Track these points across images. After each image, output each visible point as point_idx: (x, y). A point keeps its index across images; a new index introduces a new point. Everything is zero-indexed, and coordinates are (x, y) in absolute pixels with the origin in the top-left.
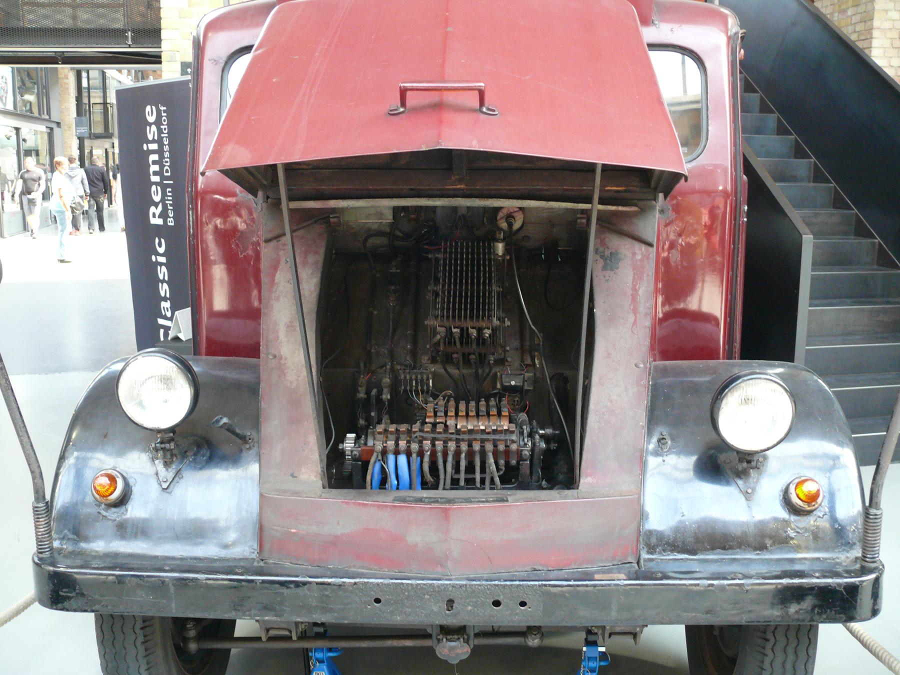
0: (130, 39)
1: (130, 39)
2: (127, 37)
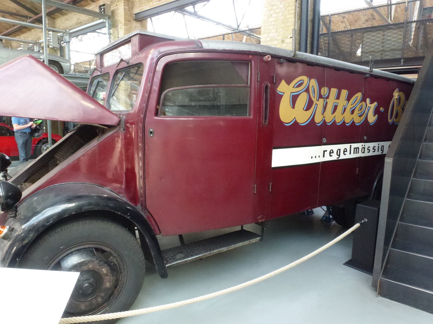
0: (402, 63)
1: (402, 63)
2: (401, 62)
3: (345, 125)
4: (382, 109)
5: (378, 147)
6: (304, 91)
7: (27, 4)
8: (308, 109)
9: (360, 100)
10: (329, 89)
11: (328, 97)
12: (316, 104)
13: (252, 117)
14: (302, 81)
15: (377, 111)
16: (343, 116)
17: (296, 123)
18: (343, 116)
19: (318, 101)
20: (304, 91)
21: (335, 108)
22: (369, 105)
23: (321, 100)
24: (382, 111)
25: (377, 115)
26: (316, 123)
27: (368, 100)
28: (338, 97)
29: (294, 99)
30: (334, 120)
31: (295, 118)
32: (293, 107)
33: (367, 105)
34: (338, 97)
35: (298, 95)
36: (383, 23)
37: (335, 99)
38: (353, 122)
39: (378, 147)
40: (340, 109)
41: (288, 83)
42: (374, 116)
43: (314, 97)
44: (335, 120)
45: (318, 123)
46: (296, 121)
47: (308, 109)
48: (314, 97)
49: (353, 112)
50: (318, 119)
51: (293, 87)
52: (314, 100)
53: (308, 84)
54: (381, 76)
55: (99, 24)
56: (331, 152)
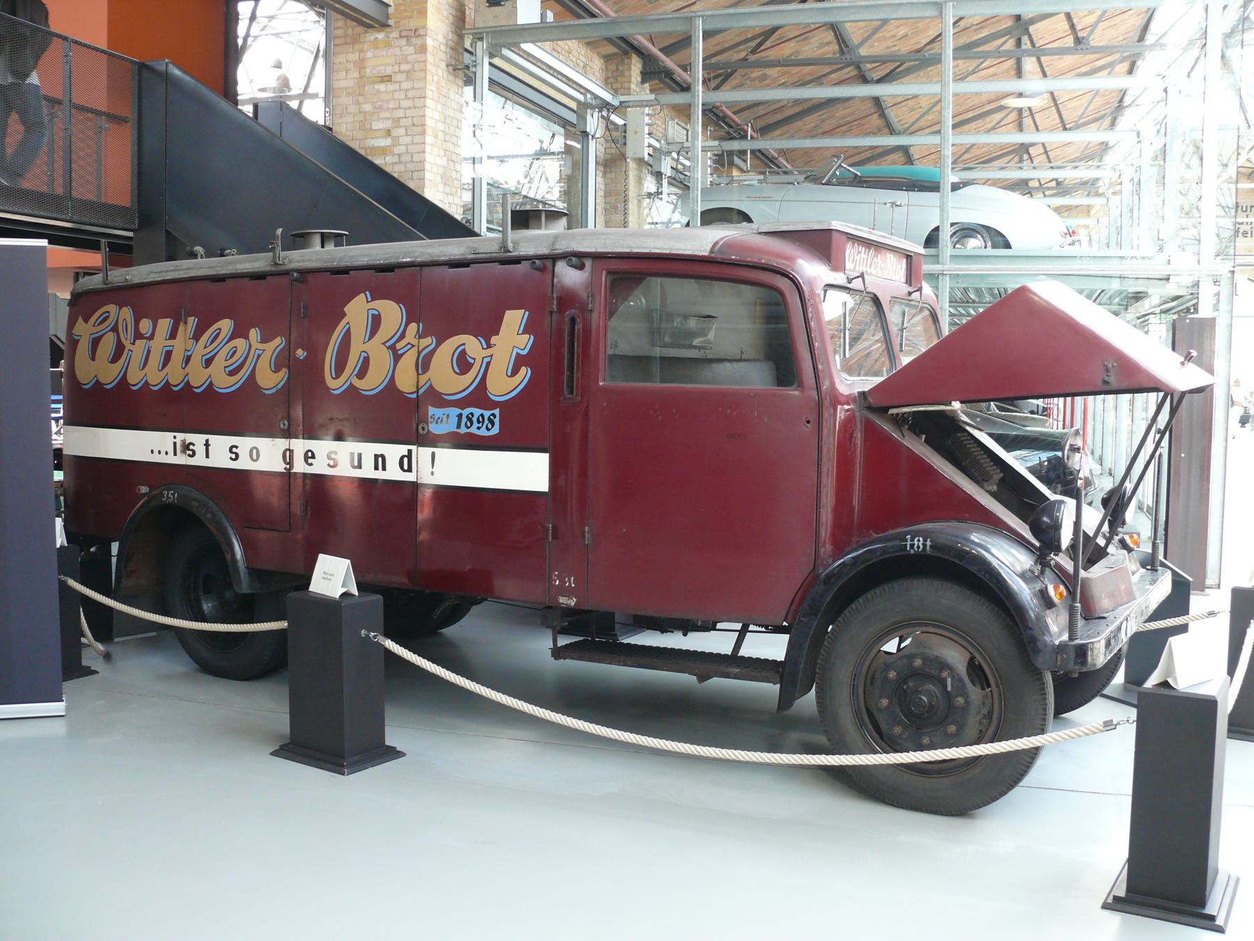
3: (193, 391)
4: (301, 353)
5: (175, 443)
6: (110, 331)
7: (307, 263)
8: (115, 359)
9: (228, 336)
10: (153, 323)
11: (151, 338)
12: (129, 350)
13: (601, 384)
14: (107, 314)
15: (284, 360)
16: (143, 373)
17: (98, 384)
18: (143, 373)
19: (133, 344)
20: (110, 331)
21: (168, 356)
22: (255, 345)
23: (141, 343)
24: (302, 358)
25: (525, 373)
26: (149, 384)
27: (254, 334)
28: (173, 336)
29: (96, 342)
30: (166, 379)
31: (429, 379)
32: (93, 359)
33: (250, 346)
34: (173, 336)
35: (100, 338)
36: (990, 31)
37: (167, 338)
38: (167, 384)
39: (175, 443)
40: (177, 358)
41: (86, 321)
42: (277, 370)
43: (126, 339)
44: (188, 381)
45: (84, 385)
46: (97, 381)
47: (115, 359)
48: (126, 339)
49: (208, 362)
50: (135, 378)
51: (94, 326)
52: (127, 343)
53: (116, 318)
54: (96, 289)
55: (238, 277)
56: (310, 454)
